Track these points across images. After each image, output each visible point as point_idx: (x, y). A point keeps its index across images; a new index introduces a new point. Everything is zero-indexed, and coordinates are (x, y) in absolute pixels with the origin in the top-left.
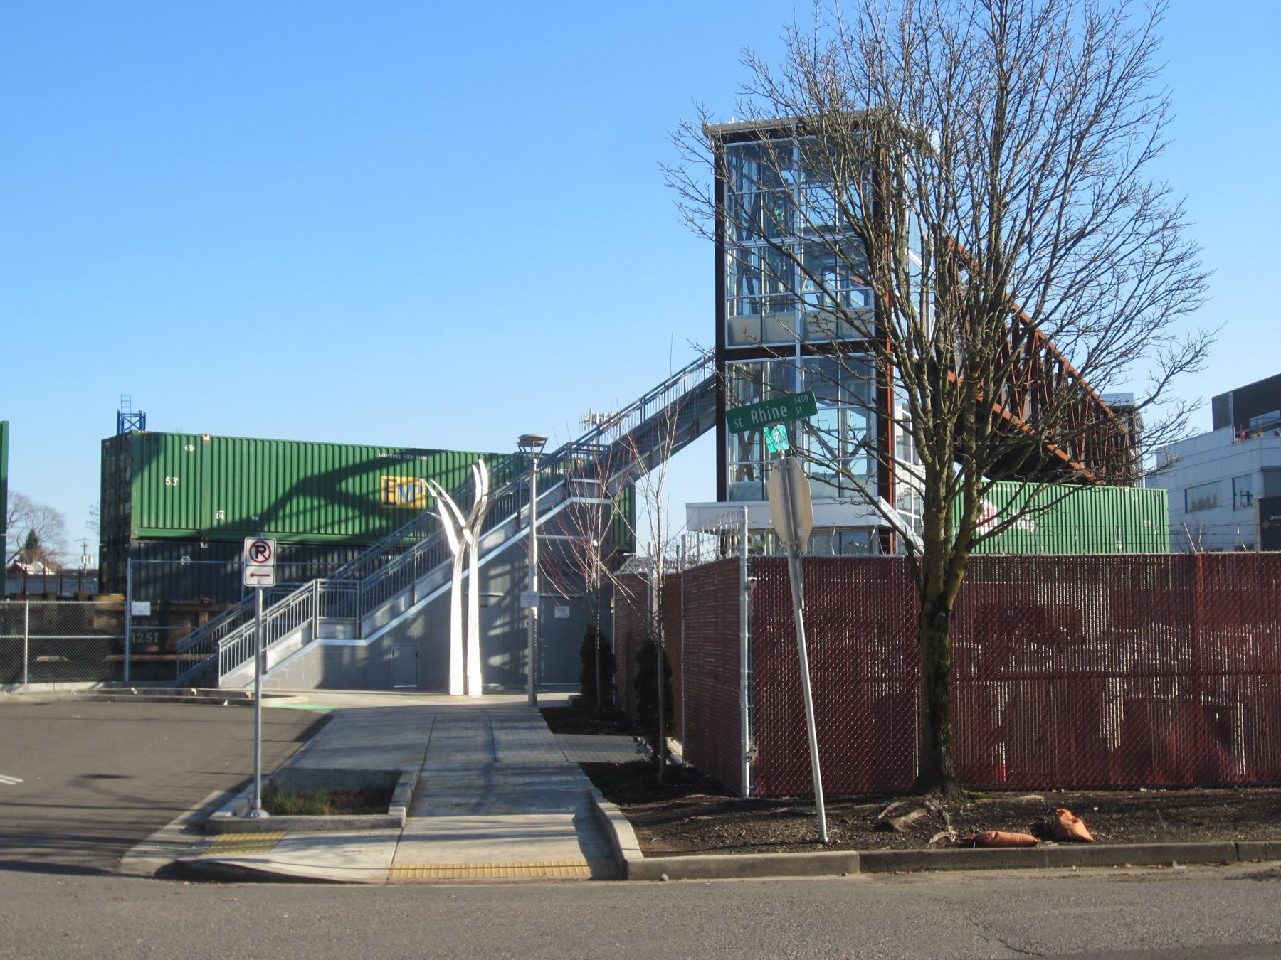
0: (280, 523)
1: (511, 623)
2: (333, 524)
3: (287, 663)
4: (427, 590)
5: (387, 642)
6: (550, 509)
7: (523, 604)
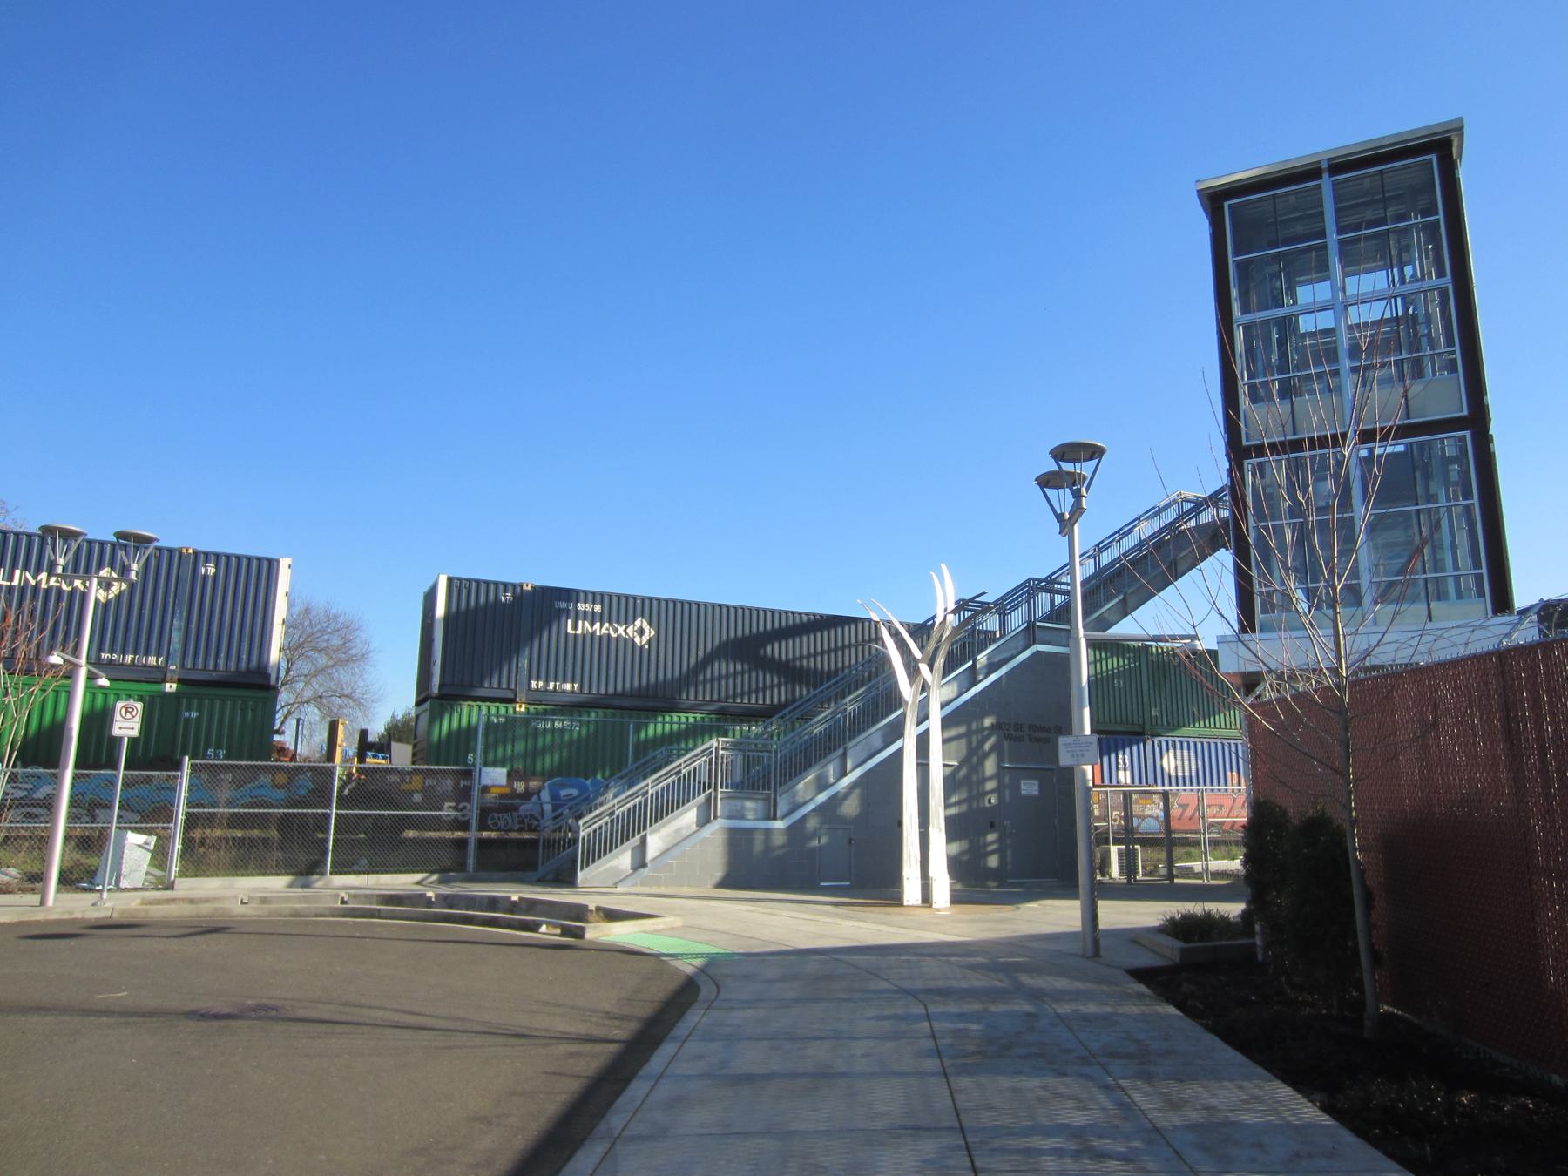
1: (968, 800)
2: (750, 693)
3: (675, 852)
4: (864, 755)
5: (812, 824)
7: (1065, 760)
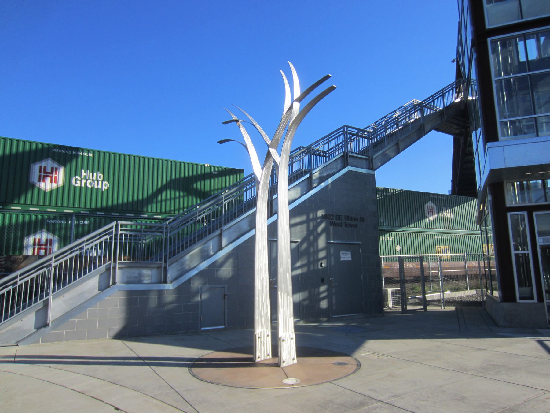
0: (154, 206)
1: (308, 265)
4: (234, 236)
6: (334, 174)
